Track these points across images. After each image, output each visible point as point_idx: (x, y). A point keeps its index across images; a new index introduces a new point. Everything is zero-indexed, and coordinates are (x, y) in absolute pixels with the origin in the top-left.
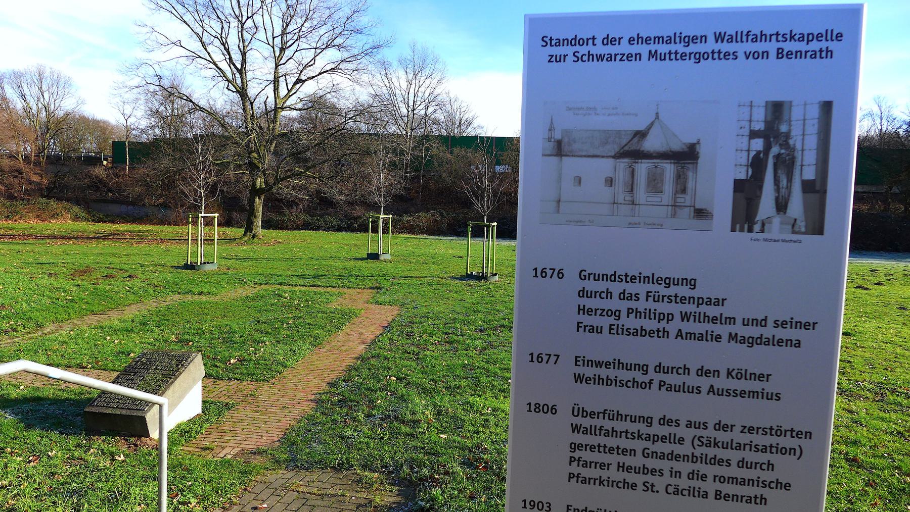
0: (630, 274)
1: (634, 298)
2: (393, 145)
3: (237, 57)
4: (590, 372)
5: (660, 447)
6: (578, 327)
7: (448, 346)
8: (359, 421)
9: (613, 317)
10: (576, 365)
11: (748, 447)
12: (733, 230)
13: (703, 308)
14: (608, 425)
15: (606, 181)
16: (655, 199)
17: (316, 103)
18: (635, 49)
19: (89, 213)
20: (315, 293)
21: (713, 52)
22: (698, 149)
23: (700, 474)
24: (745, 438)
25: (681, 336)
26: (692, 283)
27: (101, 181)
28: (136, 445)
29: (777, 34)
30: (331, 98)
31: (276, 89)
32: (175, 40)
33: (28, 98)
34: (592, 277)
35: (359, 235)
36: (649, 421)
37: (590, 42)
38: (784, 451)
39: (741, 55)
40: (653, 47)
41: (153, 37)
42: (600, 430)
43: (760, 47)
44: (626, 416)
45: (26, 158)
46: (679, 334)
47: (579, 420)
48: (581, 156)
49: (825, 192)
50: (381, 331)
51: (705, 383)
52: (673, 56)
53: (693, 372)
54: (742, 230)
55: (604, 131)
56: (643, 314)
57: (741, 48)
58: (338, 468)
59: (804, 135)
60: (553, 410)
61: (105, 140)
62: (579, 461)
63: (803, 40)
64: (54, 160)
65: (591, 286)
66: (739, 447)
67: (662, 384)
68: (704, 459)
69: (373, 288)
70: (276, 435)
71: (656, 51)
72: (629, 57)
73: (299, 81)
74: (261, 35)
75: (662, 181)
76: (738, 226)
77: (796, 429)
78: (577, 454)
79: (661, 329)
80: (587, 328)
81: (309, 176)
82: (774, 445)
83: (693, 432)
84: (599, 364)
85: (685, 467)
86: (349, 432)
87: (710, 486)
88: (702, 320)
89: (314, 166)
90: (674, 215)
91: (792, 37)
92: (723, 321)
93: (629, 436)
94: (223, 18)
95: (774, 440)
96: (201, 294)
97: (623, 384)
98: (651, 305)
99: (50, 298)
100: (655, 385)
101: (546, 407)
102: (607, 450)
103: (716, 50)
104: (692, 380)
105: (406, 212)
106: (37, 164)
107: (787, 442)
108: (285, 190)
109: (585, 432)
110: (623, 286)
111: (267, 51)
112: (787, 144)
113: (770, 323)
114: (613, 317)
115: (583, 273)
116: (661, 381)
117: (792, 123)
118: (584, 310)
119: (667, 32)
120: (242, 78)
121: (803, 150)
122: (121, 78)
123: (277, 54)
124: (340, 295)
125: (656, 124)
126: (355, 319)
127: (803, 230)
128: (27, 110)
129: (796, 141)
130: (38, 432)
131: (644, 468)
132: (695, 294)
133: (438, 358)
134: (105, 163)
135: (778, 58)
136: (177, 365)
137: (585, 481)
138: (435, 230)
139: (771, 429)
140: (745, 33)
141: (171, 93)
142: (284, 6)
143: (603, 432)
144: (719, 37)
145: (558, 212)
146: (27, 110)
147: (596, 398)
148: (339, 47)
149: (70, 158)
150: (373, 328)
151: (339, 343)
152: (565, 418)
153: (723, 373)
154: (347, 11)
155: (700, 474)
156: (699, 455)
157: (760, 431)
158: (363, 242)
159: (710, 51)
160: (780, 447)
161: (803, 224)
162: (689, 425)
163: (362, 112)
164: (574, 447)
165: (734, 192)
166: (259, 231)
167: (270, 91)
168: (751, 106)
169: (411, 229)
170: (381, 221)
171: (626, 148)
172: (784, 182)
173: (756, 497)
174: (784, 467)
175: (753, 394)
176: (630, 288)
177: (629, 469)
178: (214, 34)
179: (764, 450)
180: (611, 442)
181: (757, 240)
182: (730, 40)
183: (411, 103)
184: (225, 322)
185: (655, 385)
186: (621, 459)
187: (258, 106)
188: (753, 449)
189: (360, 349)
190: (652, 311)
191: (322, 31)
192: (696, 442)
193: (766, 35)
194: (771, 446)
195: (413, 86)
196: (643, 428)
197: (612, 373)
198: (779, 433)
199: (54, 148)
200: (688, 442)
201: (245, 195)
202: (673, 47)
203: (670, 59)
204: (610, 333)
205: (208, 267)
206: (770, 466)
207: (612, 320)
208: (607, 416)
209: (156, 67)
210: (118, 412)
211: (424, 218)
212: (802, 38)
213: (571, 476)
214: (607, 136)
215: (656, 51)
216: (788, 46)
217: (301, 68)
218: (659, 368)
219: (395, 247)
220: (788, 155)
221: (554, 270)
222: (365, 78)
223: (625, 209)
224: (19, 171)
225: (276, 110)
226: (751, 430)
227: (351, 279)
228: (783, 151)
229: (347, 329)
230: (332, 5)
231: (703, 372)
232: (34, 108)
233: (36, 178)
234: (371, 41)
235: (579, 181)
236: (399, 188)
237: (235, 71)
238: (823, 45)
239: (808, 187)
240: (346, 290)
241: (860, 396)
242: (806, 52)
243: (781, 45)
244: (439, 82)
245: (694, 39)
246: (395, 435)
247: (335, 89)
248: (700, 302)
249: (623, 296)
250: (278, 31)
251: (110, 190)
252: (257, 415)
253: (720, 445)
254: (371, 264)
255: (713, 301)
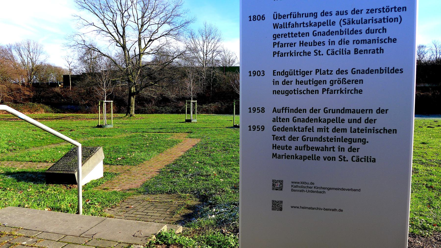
2: (198, 71)
3: (121, 30)
7: (224, 152)
17: (159, 52)
19: (53, 109)
20: (160, 135)
23: (345, 41)
24: (369, 16)
27: (58, 94)
28: (70, 188)
30: (166, 48)
31: (140, 45)
32: (91, 23)
33: (23, 55)
35: (182, 115)
36: (315, 15)
41: (80, 22)
45: (23, 84)
47: (278, 21)
50: (192, 147)
58: (169, 193)
60: (263, 18)
61: (60, 76)
64: (36, 85)
66: (366, 22)
68: (347, 32)
69: (188, 133)
70: (139, 183)
73: (150, 40)
74: (132, 19)
78: (277, 40)
82: (386, 17)
85: (337, 38)
87: (351, 47)
93: (305, 25)
94: (113, 12)
95: (385, 15)
96: (105, 136)
99: (33, 138)
101: (259, 17)
105: (205, 103)
106: (28, 86)
107: (392, 15)
108: (145, 93)
111: (135, 25)
120: (123, 40)
122: (66, 42)
123: (140, 27)
124: (172, 135)
126: (179, 143)
128: (23, 62)
130: (23, 182)
133: (220, 156)
134: (60, 85)
136: (91, 152)
137: (282, 55)
138: (218, 112)
139: (383, 8)
141: (90, 49)
142: (142, 5)
146: (23, 62)
148: (169, 23)
149: (43, 84)
150: (188, 146)
154: (173, 6)
155: (345, 41)
156: (344, 30)
157: (377, 10)
158: (183, 117)
160: (389, 18)
162: (338, 13)
163: (182, 54)
164: (276, 36)
166: (135, 115)
167: (137, 45)
169: (207, 112)
170: (192, 103)
173: (377, 49)
174: (392, 30)
177: (306, 44)
178: (110, 19)
179: (380, 21)
180: (295, 30)
183: (205, 51)
184: (116, 145)
186: (302, 39)
187: (131, 53)
189: (182, 153)
191: (161, 15)
192: (342, 23)
194: (384, 19)
195: (206, 43)
196: (312, 20)
198: (388, 10)
199: (35, 79)
200: (337, 23)
201: (126, 99)
205: (109, 126)
206: (384, 30)
208: (292, 16)
209: (82, 36)
210: (62, 172)
211: (213, 106)
213: (274, 53)
217: (151, 34)
219: (198, 119)
222: (182, 38)
224: (19, 89)
225: (140, 55)
226: (372, 11)
227: (177, 129)
229: (175, 147)
232: (26, 61)
233: (27, 93)
234: (184, 19)
236: (200, 91)
237: (120, 37)
240: (175, 134)
241: (432, 165)
244: (218, 41)
246: (198, 180)
247: (168, 43)
250: (140, 16)
251: (62, 98)
252: (130, 177)
253: (355, 22)
254: (188, 124)
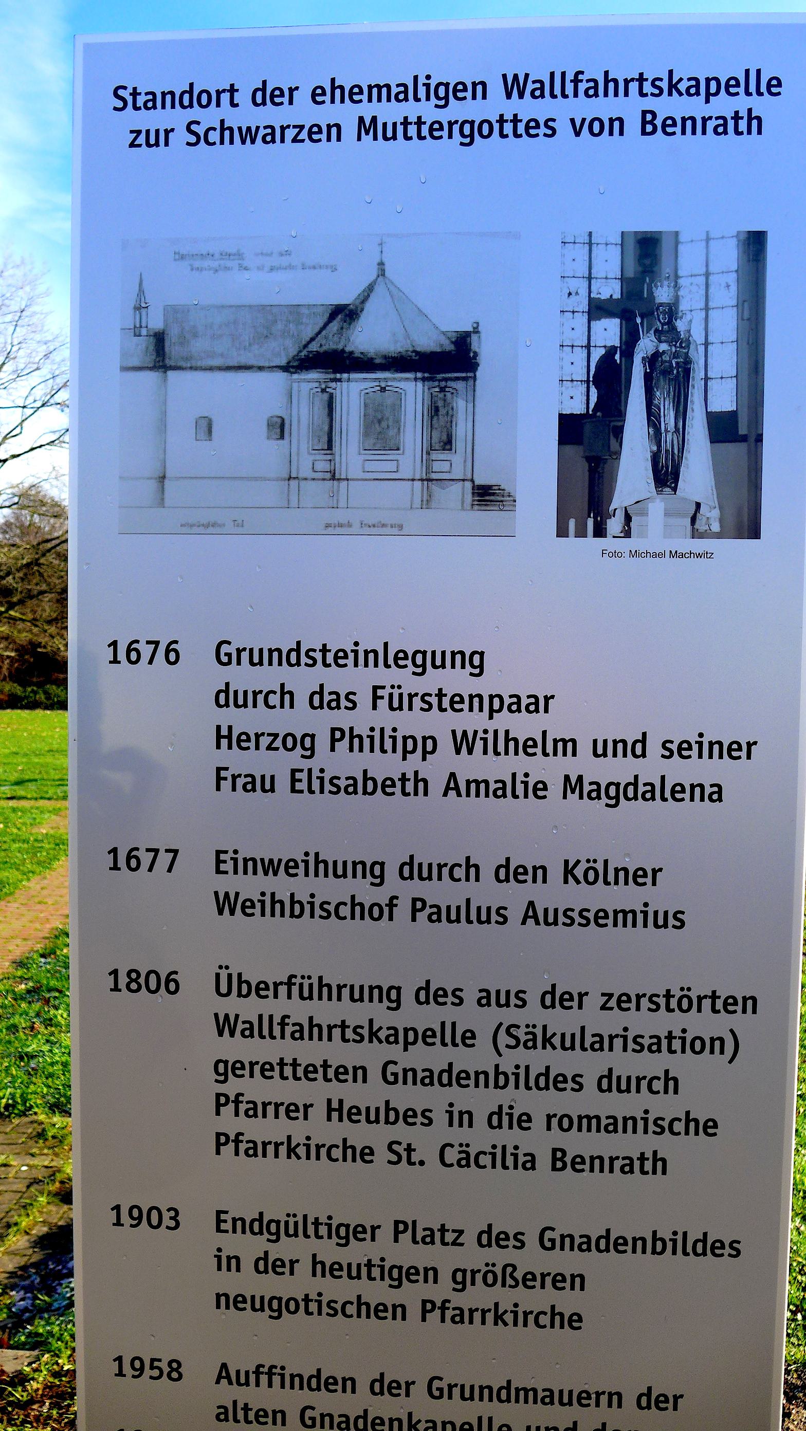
0: (333, 647)
1: (344, 703)
4: (250, 886)
5: (422, 1057)
6: (219, 779)
8: (58, 1025)
9: (299, 750)
10: (218, 871)
11: (618, 1042)
12: (562, 532)
13: (504, 721)
14: (299, 1010)
15: (270, 425)
16: (383, 465)
18: (326, 114)
20: (14, 810)
21: (501, 120)
22: (474, 347)
24: (610, 1023)
25: (457, 789)
26: (475, 662)
29: (641, 79)
34: (245, 656)
36: (391, 996)
37: (225, 97)
38: (698, 1045)
39: (564, 128)
40: (367, 110)
42: (283, 1024)
43: (604, 107)
44: (340, 988)
46: (452, 785)
47: (232, 1005)
48: (211, 369)
49: (759, 439)
51: (514, 897)
52: (412, 130)
53: (487, 873)
54: (581, 533)
55: (263, 308)
56: (367, 742)
57: (563, 110)
59: (707, 309)
60: (170, 983)
62: (237, 1102)
63: (698, 93)
65: (244, 677)
66: (600, 1043)
67: (417, 905)
68: (523, 1079)
71: (374, 119)
72: (314, 133)
75: (398, 422)
76: (572, 524)
77: (723, 993)
78: (232, 1087)
79: (410, 775)
80: (240, 782)
81: (15, 619)
82: (677, 1033)
83: (496, 1015)
84: (270, 867)
85: (481, 1100)
86: (32, 1047)
87: (539, 1141)
88: (501, 748)
89: (21, 602)
90: (427, 502)
91: (673, 87)
92: (550, 749)
93: (349, 1034)
95: (673, 1022)
97: (329, 912)
98: (384, 718)
100: (403, 909)
102: (300, 1072)
103: (508, 116)
104: (487, 892)
107: (703, 1024)
109: (249, 1032)
110: (318, 676)
112: (673, 329)
113: (654, 748)
114: (299, 750)
115: (225, 649)
116: (414, 900)
117: (680, 281)
118: (229, 737)
119: (396, 75)
121: (706, 344)
124: (57, 812)
125: (380, 289)
127: (716, 527)
129: (690, 323)
131: (388, 1109)
132: (484, 686)
135: (644, 133)
137: (253, 1150)
139: (668, 995)
140: (570, 76)
143: (289, 1030)
144: (514, 86)
145: (161, 503)
147: (268, 948)
151: (45, 892)
152: (199, 1001)
153: (556, 872)
155: (516, 1113)
156: (510, 1070)
157: (644, 1002)
159: (494, 119)
160: (689, 1037)
161: (716, 513)
162: (485, 999)
164: (226, 1069)
165: (559, 444)
168: (590, 244)
171: (314, 347)
172: (669, 419)
174: (703, 1082)
175: (625, 917)
176: (337, 680)
179: (656, 1046)
180: (309, 1052)
181: (615, 554)
182: (539, 93)
185: (403, 909)
186: (335, 1091)
188: (631, 1046)
190: (388, 732)
191: (36, 378)
192: (503, 1039)
193: (615, 81)
197: (302, 886)
198: (685, 1005)
200: (484, 1040)
202: (411, 110)
203: (407, 138)
204: (293, 790)
206: (671, 1082)
207: (295, 759)
208: (295, 990)
212: (694, 89)
213: (221, 1141)
214: (268, 318)
215: (374, 119)
216: (666, 106)
218: (410, 869)
220: (676, 355)
221: (157, 643)
223: (316, 491)
226: (623, 1001)
228: (664, 347)
230: (50, 338)
231: (508, 872)
235: (207, 427)
238: (741, 103)
239: (723, 429)
242: (705, 120)
243: (650, 103)
245: (457, 91)
248: (494, 705)
249: (320, 699)
253: (556, 1041)
255: (525, 702)
